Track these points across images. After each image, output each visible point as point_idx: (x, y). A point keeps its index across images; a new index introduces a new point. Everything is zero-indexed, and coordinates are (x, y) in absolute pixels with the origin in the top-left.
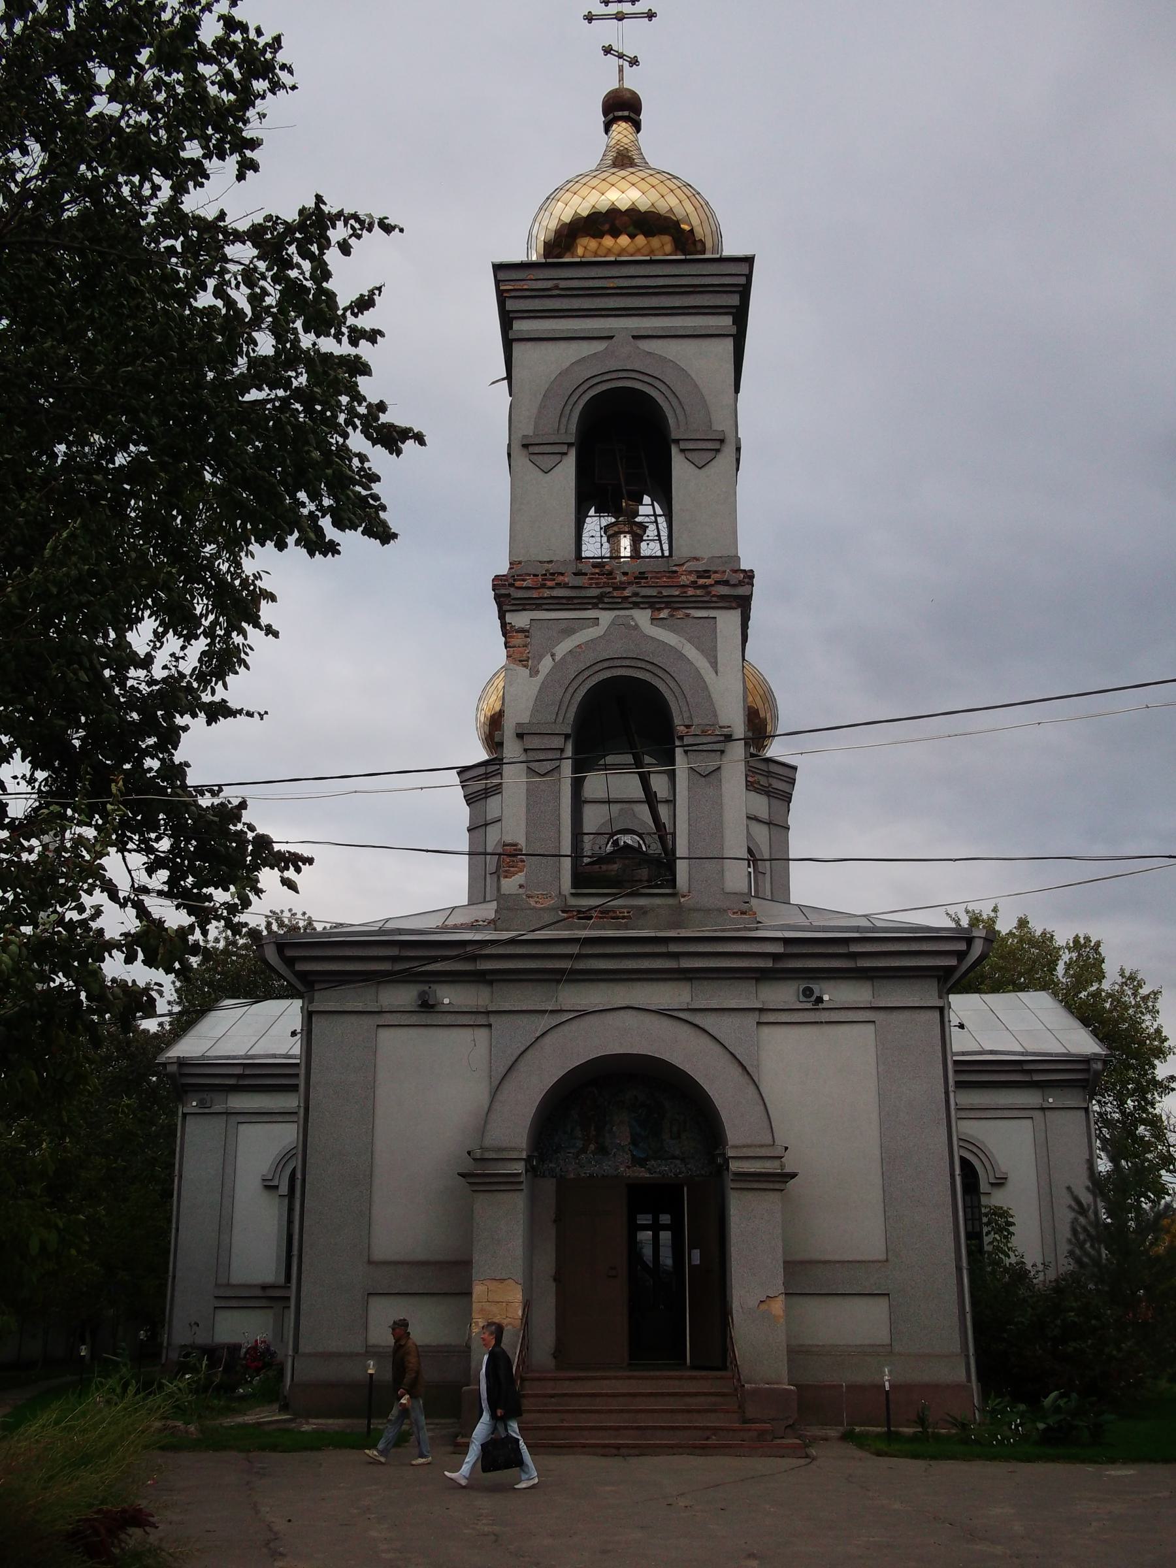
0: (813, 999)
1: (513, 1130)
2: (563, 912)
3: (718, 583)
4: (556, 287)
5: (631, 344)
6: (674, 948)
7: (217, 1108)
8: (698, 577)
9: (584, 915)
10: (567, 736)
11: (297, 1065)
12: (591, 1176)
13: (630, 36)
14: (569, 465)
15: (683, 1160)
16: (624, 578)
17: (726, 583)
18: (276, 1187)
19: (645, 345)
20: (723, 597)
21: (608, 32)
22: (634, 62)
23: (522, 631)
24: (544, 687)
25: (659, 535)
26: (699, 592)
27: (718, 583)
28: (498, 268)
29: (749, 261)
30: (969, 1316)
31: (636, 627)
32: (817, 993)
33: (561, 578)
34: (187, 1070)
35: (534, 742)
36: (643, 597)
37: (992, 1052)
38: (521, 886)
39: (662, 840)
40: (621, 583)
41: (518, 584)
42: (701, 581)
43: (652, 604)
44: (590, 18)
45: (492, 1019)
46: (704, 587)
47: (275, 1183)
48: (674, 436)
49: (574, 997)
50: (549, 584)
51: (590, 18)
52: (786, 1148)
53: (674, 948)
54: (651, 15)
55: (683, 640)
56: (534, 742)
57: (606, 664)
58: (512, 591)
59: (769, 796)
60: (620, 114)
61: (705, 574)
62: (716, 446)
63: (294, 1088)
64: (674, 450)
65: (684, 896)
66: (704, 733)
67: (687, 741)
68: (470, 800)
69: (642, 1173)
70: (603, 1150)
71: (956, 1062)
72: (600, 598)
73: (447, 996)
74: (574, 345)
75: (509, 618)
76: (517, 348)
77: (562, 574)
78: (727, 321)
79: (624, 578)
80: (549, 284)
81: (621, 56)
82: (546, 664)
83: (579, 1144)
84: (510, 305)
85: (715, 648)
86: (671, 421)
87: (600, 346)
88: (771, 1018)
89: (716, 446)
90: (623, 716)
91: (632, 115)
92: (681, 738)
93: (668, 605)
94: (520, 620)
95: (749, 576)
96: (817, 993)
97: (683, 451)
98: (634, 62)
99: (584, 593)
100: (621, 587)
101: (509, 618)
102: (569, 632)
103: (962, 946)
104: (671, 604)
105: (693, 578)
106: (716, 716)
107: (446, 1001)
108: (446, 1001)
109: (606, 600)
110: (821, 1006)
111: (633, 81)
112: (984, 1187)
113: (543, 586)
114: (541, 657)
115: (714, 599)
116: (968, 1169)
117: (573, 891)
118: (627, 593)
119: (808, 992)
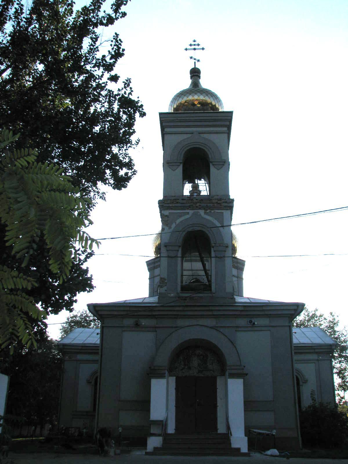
0: (252, 324)
1: (163, 359)
2: (178, 298)
3: (224, 202)
5: (199, 135)
6: (211, 308)
9: (185, 299)
10: (179, 246)
11: (98, 346)
13: (197, 54)
15: (213, 371)
16: (197, 201)
18: (91, 382)
19: (202, 135)
20: (225, 206)
21: (191, 53)
22: (198, 61)
23: (166, 216)
25: (206, 189)
26: (218, 205)
27: (224, 202)
28: (161, 114)
29: (231, 113)
30: (298, 417)
31: (200, 215)
32: (253, 322)
33: (178, 201)
34: (66, 347)
37: (303, 344)
38: (166, 290)
39: (207, 278)
41: (166, 202)
43: (205, 208)
44: (186, 49)
47: (91, 381)
49: (180, 322)
50: (174, 202)
51: (186, 49)
53: (211, 308)
54: (203, 49)
59: (238, 269)
60: (195, 74)
61: (220, 199)
63: (98, 353)
64: (211, 165)
65: (214, 293)
68: (149, 270)
69: (201, 375)
70: (190, 368)
71: (294, 346)
72: (190, 207)
73: (144, 322)
74: (177, 136)
76: (166, 137)
78: (225, 129)
79: (197, 201)
80: (175, 119)
81: (195, 59)
82: (174, 226)
84: (164, 124)
85: (223, 219)
86: (210, 156)
87: (189, 135)
88: (240, 329)
90: (197, 236)
91: (198, 75)
93: (209, 209)
96: (253, 322)
97: (213, 165)
98: (198, 61)
100: (196, 203)
102: (180, 216)
103: (296, 308)
104: (211, 208)
106: (223, 240)
108: (143, 324)
109: (191, 207)
110: (254, 325)
112: (301, 383)
113: (173, 203)
115: (223, 207)
116: (298, 379)
117: (181, 292)
118: (198, 205)
119: (251, 322)
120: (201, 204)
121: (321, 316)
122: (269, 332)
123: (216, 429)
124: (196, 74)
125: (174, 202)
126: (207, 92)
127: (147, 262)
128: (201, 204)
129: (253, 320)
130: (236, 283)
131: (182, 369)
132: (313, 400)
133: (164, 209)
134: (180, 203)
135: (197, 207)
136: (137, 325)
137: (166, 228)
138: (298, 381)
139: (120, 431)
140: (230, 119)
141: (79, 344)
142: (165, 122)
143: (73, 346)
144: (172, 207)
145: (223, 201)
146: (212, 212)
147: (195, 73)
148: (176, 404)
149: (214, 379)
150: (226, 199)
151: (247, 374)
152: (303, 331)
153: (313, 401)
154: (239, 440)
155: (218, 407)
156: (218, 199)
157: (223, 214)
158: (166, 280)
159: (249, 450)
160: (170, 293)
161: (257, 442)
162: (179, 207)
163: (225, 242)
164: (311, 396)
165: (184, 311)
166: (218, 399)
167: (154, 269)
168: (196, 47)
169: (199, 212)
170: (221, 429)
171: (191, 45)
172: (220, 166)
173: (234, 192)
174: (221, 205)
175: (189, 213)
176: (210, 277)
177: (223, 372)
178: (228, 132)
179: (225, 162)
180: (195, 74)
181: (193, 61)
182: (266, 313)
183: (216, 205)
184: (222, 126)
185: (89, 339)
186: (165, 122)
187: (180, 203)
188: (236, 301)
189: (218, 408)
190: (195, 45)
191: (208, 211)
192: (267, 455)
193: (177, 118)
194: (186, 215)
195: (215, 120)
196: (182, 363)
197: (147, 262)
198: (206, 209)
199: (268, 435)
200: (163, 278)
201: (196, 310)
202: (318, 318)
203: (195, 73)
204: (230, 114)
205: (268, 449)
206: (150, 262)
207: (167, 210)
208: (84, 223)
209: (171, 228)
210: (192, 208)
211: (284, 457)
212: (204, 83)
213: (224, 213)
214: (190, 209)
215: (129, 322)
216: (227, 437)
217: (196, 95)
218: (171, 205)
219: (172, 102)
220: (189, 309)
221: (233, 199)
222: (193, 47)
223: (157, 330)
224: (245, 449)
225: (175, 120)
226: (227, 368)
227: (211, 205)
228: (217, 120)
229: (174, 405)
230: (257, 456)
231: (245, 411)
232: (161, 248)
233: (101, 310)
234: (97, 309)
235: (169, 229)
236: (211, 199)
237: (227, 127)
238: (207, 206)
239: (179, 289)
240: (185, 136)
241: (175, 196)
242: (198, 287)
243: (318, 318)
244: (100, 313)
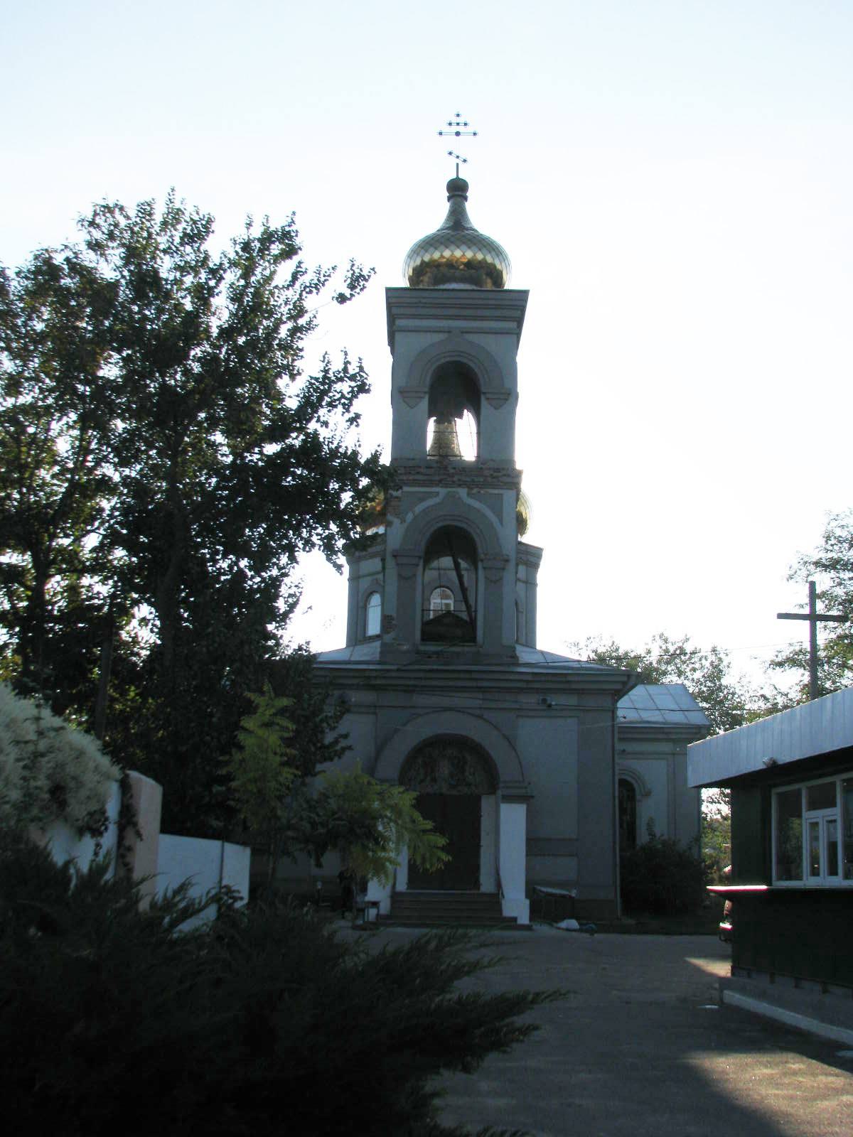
9: (429, 655)
13: (463, 146)
19: (470, 337)
21: (450, 142)
22: (465, 161)
28: (388, 290)
42: (495, 474)
43: (469, 486)
46: (497, 477)
49: (421, 700)
60: (457, 193)
61: (498, 470)
65: (481, 647)
69: (454, 792)
70: (434, 780)
72: (440, 481)
76: (398, 336)
78: (514, 325)
81: (458, 157)
84: (395, 311)
93: (477, 486)
96: (549, 702)
97: (488, 399)
98: (465, 161)
100: (452, 475)
102: (422, 500)
103: (625, 679)
114: (407, 513)
118: (455, 479)
119: (544, 701)
121: (693, 653)
123: (477, 884)
124: (460, 193)
125: (413, 472)
126: (480, 241)
129: (548, 698)
130: (522, 593)
132: (650, 834)
134: (422, 474)
138: (628, 793)
139: (319, 887)
147: (457, 190)
149: (478, 799)
152: (651, 692)
154: (516, 905)
158: (393, 619)
159: (531, 920)
161: (545, 907)
163: (504, 552)
165: (426, 679)
166: (483, 834)
169: (458, 493)
170: (486, 885)
173: (522, 459)
174: (499, 481)
176: (473, 614)
177: (493, 787)
179: (509, 394)
180: (457, 193)
182: (574, 686)
183: (489, 479)
184: (504, 319)
188: (522, 661)
189: (482, 850)
191: (475, 491)
192: (559, 928)
199: (563, 896)
202: (687, 657)
203: (457, 190)
204: (521, 298)
205: (563, 919)
208: (448, 853)
211: (586, 931)
212: (479, 217)
213: (505, 498)
216: (495, 899)
223: (377, 711)
224: (524, 919)
227: (482, 480)
230: (543, 929)
231: (527, 855)
236: (481, 468)
238: (473, 481)
240: (437, 338)
241: (413, 459)
242: (453, 630)
243: (687, 657)
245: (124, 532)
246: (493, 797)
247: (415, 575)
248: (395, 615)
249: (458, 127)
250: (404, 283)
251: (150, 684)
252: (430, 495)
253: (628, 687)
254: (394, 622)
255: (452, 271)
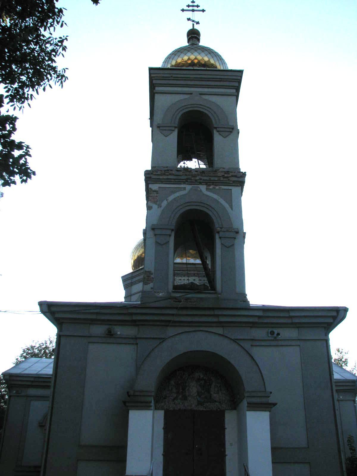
1: (149, 381)
3: (232, 176)
4: (171, 77)
6: (217, 312)
7: (23, 394)
8: (225, 174)
10: (172, 230)
12: (179, 410)
13: (196, 16)
14: (175, 134)
15: (220, 402)
16: (196, 173)
17: (236, 176)
19: (206, 97)
20: (234, 182)
21: (189, 14)
22: (198, 23)
24: (163, 212)
26: (225, 179)
27: (232, 176)
28: (151, 69)
29: (241, 72)
31: (201, 191)
35: (158, 232)
36: (203, 180)
38: (152, 288)
40: (195, 174)
41: (154, 173)
42: (226, 175)
43: (207, 183)
44: (183, 10)
45: (138, 341)
46: (227, 177)
47: (44, 424)
48: (215, 126)
49: (171, 331)
50: (167, 174)
51: (183, 10)
52: (271, 393)
55: (219, 197)
56: (158, 232)
57: (189, 204)
58: (152, 175)
61: (228, 172)
62: (231, 130)
64: (215, 132)
65: (219, 294)
66: (227, 231)
67: (221, 233)
69: (201, 408)
73: (119, 331)
75: (150, 186)
76: (157, 96)
77: (171, 170)
79: (196, 173)
83: (175, 396)
84: (154, 82)
85: (231, 200)
87: (186, 96)
89: (231, 130)
91: (197, 36)
92: (218, 232)
94: (154, 187)
95: (244, 175)
97: (218, 131)
98: (198, 23)
99: (180, 177)
101: (150, 186)
102: (173, 192)
103: (334, 314)
104: (214, 183)
105: (223, 174)
106: (232, 224)
107: (119, 333)
108: (119, 333)
109: (189, 181)
111: (196, 27)
113: (164, 174)
114: (162, 201)
115: (231, 182)
117: (173, 290)
118: (197, 178)
119: (272, 333)
120: (202, 177)
122: (297, 348)
124: (195, 36)
127: (122, 277)
128: (202, 177)
131: (174, 399)
133: (153, 182)
134: (173, 175)
135: (196, 180)
136: (110, 334)
137: (155, 207)
140: (237, 87)
141: (31, 374)
142: (156, 79)
143: (23, 377)
144: (162, 180)
145: (231, 174)
146: (217, 188)
147: (193, 35)
148: (164, 451)
150: (235, 172)
151: (274, 404)
153: (352, 451)
155: (227, 457)
156: (224, 172)
157: (231, 191)
158: (152, 274)
160: (158, 292)
162: (173, 180)
164: (348, 445)
167: (132, 286)
168: (195, 8)
169: (199, 187)
171: (188, 6)
172: (227, 134)
174: (229, 180)
175: (185, 188)
178: (236, 94)
179: (233, 129)
180: (193, 36)
181: (191, 23)
183: (222, 179)
185: (44, 369)
186: (156, 79)
187: (173, 175)
189: (226, 431)
190: (193, 6)
191: (211, 187)
193: (172, 75)
194: (181, 190)
195: (221, 80)
196: (174, 390)
197: (122, 277)
198: (209, 184)
200: (149, 272)
201: (196, 315)
203: (193, 35)
206: (127, 277)
207: (156, 183)
209: (161, 207)
210: (191, 182)
213: (232, 190)
214: (186, 183)
215: (99, 330)
217: (196, 52)
218: (161, 177)
219: (165, 62)
220: (185, 312)
221: (245, 172)
222: (191, 8)
225: (169, 77)
226: (246, 395)
228: (223, 80)
229: (162, 452)
231: (273, 463)
232: (147, 233)
233: (58, 312)
234: (53, 309)
235: (158, 208)
237: (235, 89)
239: (171, 287)
244: (57, 316)
245: (7, 59)
246: (235, 411)
247: (168, 242)
248: (153, 271)
249: (193, 7)
250: (149, 168)
251: (37, 59)
252: (180, 189)
253: (339, 319)
254: (152, 276)
255: (180, 279)
